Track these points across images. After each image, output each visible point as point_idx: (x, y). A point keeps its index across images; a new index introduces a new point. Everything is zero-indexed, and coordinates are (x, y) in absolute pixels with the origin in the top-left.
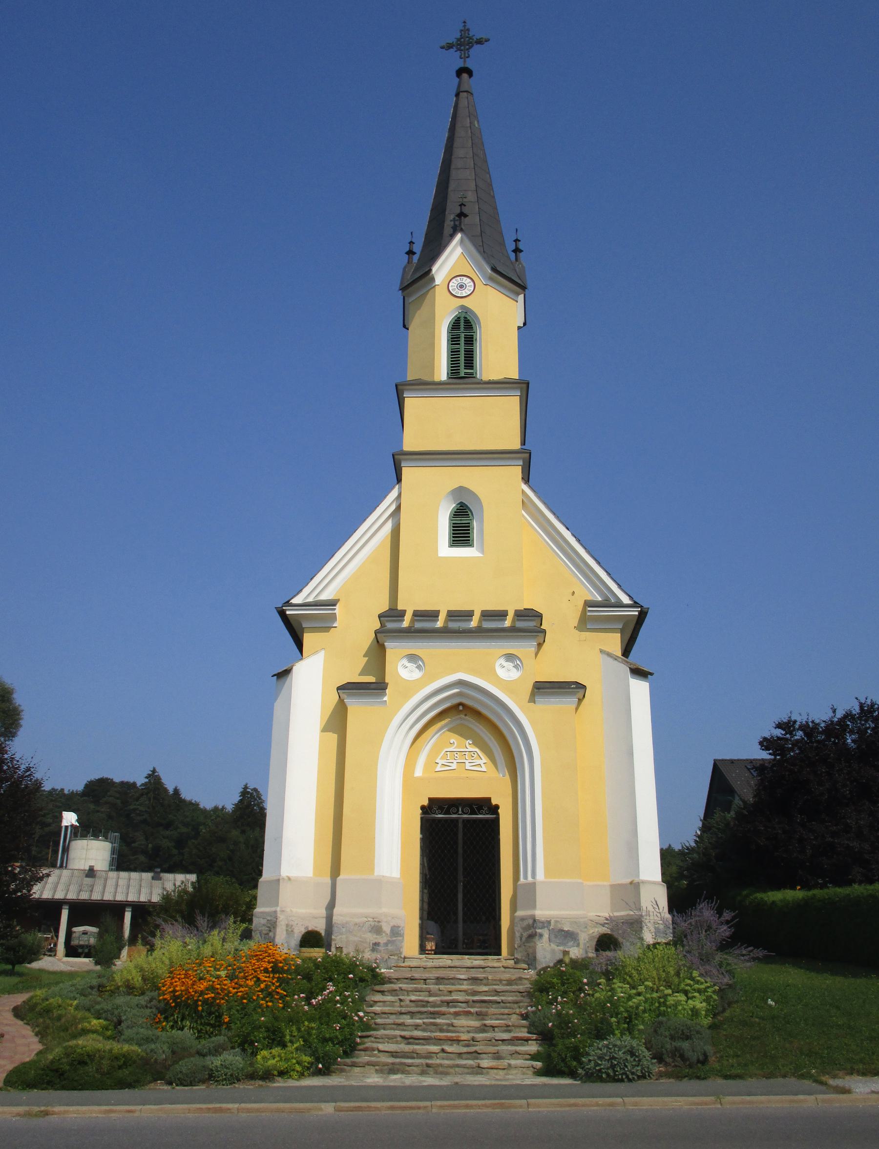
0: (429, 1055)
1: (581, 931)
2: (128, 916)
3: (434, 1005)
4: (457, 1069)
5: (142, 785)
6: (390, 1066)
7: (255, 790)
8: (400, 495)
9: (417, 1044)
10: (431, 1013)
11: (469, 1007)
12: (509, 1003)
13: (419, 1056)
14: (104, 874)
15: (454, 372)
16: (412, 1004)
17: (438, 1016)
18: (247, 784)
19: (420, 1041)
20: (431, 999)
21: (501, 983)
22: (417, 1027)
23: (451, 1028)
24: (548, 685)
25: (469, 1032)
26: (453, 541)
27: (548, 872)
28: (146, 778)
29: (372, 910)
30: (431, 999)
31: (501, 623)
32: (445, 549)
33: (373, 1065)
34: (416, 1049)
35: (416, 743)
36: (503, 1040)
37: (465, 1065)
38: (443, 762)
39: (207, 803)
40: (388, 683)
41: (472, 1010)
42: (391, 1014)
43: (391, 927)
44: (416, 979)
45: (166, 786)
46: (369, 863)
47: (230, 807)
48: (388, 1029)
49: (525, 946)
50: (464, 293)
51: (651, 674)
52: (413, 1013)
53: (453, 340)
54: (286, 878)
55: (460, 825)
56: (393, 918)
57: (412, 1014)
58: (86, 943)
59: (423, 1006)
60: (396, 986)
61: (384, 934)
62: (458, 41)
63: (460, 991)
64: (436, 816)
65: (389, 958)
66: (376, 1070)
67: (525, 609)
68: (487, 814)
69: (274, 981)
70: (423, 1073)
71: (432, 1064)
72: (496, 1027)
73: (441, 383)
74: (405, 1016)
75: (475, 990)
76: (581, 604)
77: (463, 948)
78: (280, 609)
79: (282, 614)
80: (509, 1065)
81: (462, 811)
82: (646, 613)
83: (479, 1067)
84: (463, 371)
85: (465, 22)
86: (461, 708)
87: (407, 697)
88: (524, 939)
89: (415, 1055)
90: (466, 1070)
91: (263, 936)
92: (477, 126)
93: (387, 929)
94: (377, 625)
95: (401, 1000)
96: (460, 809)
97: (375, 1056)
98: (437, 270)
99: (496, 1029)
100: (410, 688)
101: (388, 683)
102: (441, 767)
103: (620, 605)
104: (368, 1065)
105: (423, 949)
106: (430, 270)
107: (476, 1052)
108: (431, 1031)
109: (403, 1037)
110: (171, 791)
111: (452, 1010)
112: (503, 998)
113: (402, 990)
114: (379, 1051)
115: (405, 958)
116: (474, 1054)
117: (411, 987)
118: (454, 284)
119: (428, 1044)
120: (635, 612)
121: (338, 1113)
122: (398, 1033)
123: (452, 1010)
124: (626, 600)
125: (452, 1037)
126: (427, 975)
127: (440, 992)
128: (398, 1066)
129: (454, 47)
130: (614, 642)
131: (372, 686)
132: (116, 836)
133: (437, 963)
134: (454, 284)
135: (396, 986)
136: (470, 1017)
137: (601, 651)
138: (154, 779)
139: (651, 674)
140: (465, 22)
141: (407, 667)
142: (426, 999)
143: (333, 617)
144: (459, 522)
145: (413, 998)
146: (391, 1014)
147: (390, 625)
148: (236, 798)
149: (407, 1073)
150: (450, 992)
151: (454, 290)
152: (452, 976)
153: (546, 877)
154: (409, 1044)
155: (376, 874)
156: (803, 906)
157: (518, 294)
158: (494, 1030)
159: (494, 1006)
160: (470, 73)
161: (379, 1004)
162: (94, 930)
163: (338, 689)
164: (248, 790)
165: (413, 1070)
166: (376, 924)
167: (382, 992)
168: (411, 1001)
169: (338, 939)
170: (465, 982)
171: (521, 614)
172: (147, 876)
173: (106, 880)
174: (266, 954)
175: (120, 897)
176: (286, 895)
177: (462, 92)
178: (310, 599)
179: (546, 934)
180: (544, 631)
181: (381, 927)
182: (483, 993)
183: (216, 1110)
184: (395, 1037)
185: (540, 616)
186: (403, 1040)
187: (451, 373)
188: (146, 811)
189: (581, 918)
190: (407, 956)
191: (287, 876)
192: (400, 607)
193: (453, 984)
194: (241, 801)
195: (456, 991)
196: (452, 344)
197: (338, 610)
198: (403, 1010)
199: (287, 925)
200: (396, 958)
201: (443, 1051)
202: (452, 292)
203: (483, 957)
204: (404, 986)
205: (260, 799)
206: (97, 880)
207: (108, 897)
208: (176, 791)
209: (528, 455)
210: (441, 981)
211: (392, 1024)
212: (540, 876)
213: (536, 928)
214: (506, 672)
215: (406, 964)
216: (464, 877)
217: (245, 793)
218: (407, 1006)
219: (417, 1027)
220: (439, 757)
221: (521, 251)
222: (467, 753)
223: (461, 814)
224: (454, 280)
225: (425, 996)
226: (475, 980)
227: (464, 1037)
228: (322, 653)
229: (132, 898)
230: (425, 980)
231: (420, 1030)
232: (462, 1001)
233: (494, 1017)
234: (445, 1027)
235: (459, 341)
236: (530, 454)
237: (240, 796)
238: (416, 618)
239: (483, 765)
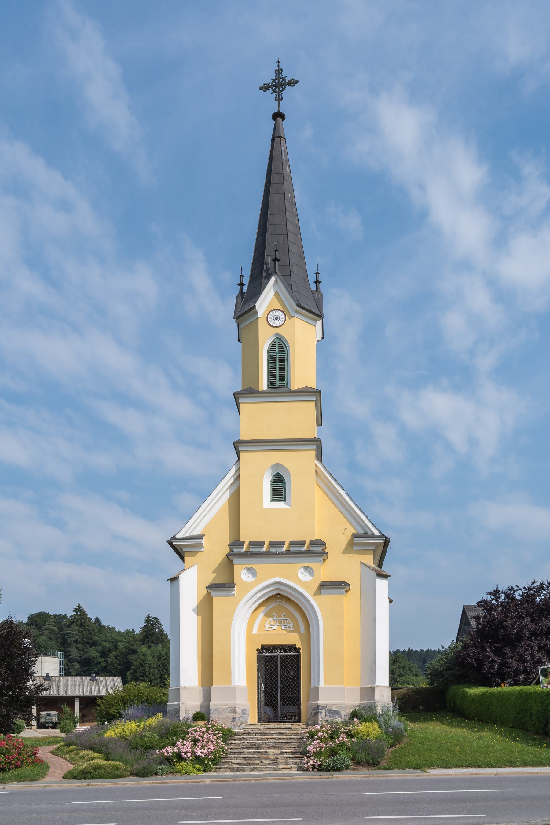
0: (255, 764)
1: (342, 710)
2: (77, 704)
3: (259, 744)
4: (267, 769)
5: (71, 616)
6: (237, 769)
7: (156, 618)
8: (237, 479)
9: (250, 760)
10: (257, 748)
11: (276, 745)
12: (296, 743)
13: (250, 764)
14: (57, 678)
15: (272, 384)
16: (249, 744)
17: (260, 749)
18: (149, 615)
19: (251, 759)
20: (258, 742)
21: (293, 735)
22: (250, 753)
23: (266, 753)
24: (328, 584)
25: (274, 755)
26: (273, 498)
27: (325, 683)
28: (74, 611)
29: (231, 702)
30: (258, 742)
31: (302, 548)
32: (268, 503)
33: (229, 769)
34: (249, 762)
35: (255, 612)
36: (290, 758)
37: (271, 767)
38: (269, 625)
39: (121, 628)
40: (235, 584)
41: (277, 746)
42: (238, 748)
43: (242, 710)
44: (251, 734)
45: (89, 616)
46: (229, 679)
47: (138, 631)
48: (236, 755)
49: (313, 718)
50: (278, 323)
51: (390, 576)
52: (248, 748)
53: (271, 359)
54: (184, 687)
55: (279, 659)
57: (248, 748)
58: (51, 721)
59: (254, 745)
60: (241, 737)
61: (238, 714)
62: (273, 82)
63: (272, 738)
64: (265, 654)
65: (241, 725)
66: (231, 770)
67: (316, 540)
68: (294, 653)
70: (252, 771)
71: (256, 767)
72: (288, 753)
73: (263, 392)
74: (245, 749)
75: (279, 738)
76: (350, 535)
77: (281, 719)
78: (169, 542)
79: (171, 544)
80: (291, 767)
81: (280, 651)
82: (389, 541)
83: (277, 768)
84: (278, 383)
85: (278, 62)
86: (278, 596)
87: (247, 591)
88: (312, 715)
89: (249, 764)
90: (271, 769)
91: (173, 716)
92: (288, 171)
93: (239, 711)
94: (227, 550)
95: (243, 743)
97: (231, 765)
98: (258, 308)
99: (287, 754)
100: (248, 587)
101: (235, 584)
102: (268, 628)
103: (373, 536)
104: (227, 768)
105: (260, 720)
106: (254, 307)
107: (277, 762)
108: (257, 755)
109: (244, 758)
110: (93, 620)
111: (267, 746)
112: (292, 741)
113: (244, 738)
114: (232, 763)
115: (249, 725)
116: (276, 763)
117: (248, 737)
118: (271, 316)
119: (255, 760)
120: (382, 541)
121: (212, 783)
122: (241, 756)
123: (267, 746)
124: (377, 533)
125: (266, 757)
126: (257, 732)
127: (262, 739)
128: (240, 768)
129: (270, 89)
130: (369, 559)
131: (226, 586)
132: (61, 653)
133: (266, 727)
134: (271, 316)
135: (241, 737)
136: (276, 749)
137: (361, 563)
138: (79, 611)
139: (390, 576)
140: (278, 62)
141: (246, 574)
142: (255, 742)
143: (202, 546)
144: (277, 486)
145: (249, 742)
146: (238, 748)
147: (236, 550)
148: (143, 625)
149: (245, 771)
150: (267, 739)
151: (271, 321)
152: (269, 732)
153: (324, 684)
154: (246, 760)
155: (232, 684)
156: (483, 695)
157: (317, 321)
158: (286, 754)
159: (288, 744)
160: (283, 117)
161: (232, 744)
162: (56, 713)
163: (206, 588)
164: (151, 619)
165: (247, 770)
166: (233, 709)
167: (234, 740)
168: (248, 743)
169: (214, 716)
170: (275, 735)
171: (313, 543)
172: (86, 679)
173: (59, 682)
175: (70, 692)
176: (183, 695)
177: (277, 137)
178: (187, 535)
179: (324, 712)
180: (327, 553)
181: (236, 710)
182: (283, 739)
183: (161, 783)
184: (240, 757)
185: (325, 544)
186: (243, 759)
187: (270, 384)
188: (76, 634)
189: (343, 704)
190: (251, 724)
191: (184, 687)
192: (241, 540)
193: (269, 736)
194: (146, 626)
195: (271, 738)
196: (270, 363)
197: (204, 541)
198: (244, 747)
199: (186, 710)
200: (245, 724)
201: (261, 762)
202: (270, 323)
203: (291, 724)
204: (245, 737)
205: (160, 624)
206: (53, 683)
207: (62, 692)
208: (97, 620)
209: (320, 442)
210: (264, 734)
211: (238, 752)
212: (322, 684)
213: (318, 709)
214: (304, 576)
215: (250, 727)
217: (148, 620)
218: (246, 745)
219: (250, 753)
221: (320, 282)
222: (282, 621)
223: (280, 653)
224: (271, 313)
225: (255, 741)
226: (280, 734)
227: (271, 757)
228: (196, 566)
229: (78, 692)
230: (255, 734)
231: (251, 754)
232: (272, 742)
233: (287, 749)
234: (263, 753)
235: (275, 360)
236: (321, 441)
237: (145, 623)
238: (250, 546)
239: (291, 627)
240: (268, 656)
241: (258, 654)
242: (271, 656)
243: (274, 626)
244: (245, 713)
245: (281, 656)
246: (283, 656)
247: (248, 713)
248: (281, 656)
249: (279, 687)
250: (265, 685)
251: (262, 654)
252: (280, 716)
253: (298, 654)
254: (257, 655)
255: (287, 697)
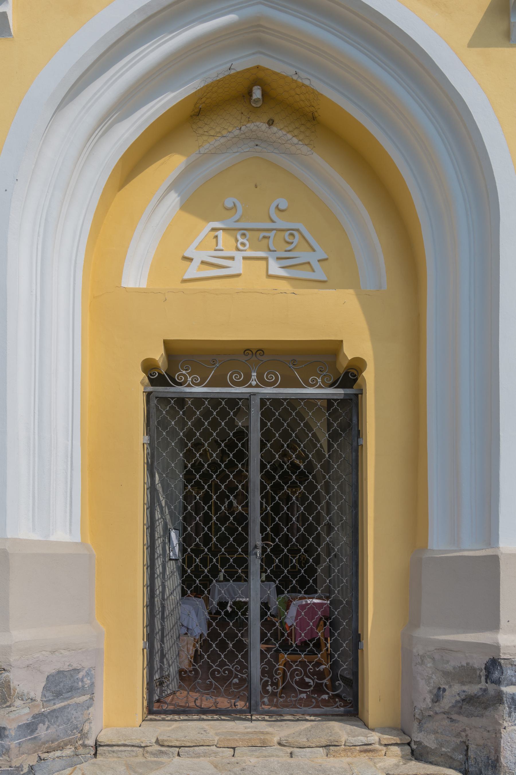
38: (206, 255)
55: (255, 404)
56: (53, 652)
64: (188, 390)
69: (166, 688)
81: (260, 377)
88: (447, 702)
96: (254, 374)
102: (199, 269)
174: (170, 662)
190: (103, 739)
213: (498, 682)
216: (263, 540)
220: (196, 243)
222: (272, 234)
223: (257, 386)
240: (198, 401)
241: (150, 389)
242: (215, 401)
243: (232, 258)
244: (71, 689)
245: (263, 401)
246: (276, 402)
247: (92, 684)
248: (263, 401)
249: (256, 547)
250: (184, 540)
251: (171, 389)
252: (260, 687)
253: (349, 391)
254: (148, 395)
255: (206, 417)
